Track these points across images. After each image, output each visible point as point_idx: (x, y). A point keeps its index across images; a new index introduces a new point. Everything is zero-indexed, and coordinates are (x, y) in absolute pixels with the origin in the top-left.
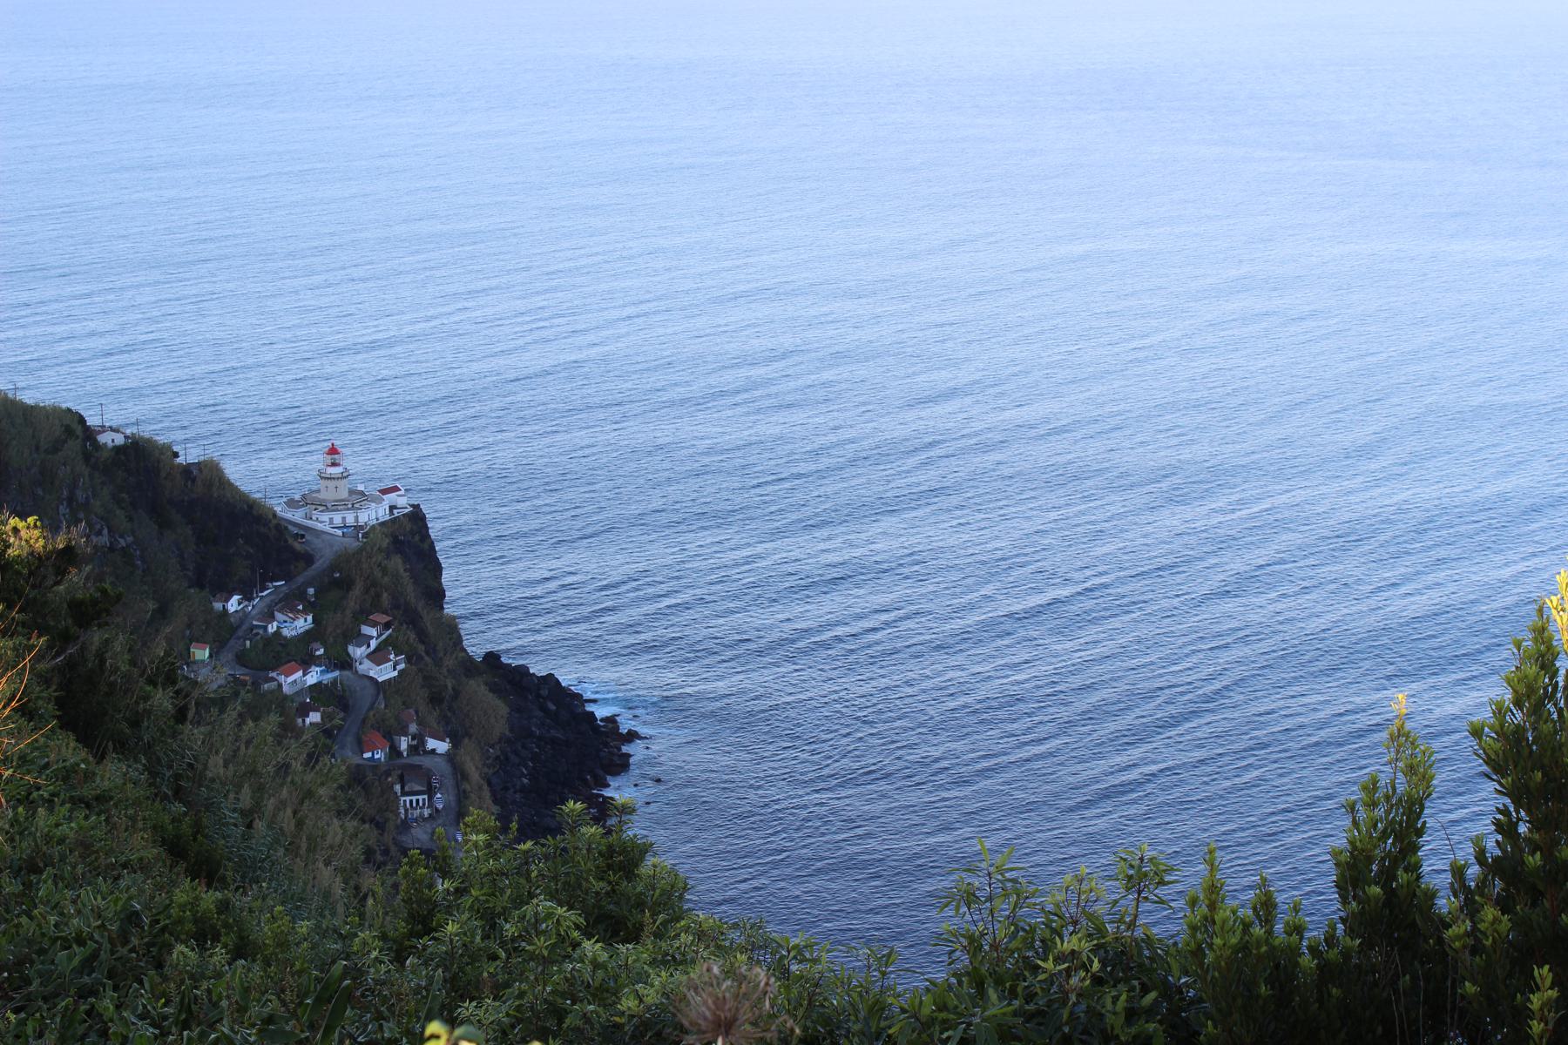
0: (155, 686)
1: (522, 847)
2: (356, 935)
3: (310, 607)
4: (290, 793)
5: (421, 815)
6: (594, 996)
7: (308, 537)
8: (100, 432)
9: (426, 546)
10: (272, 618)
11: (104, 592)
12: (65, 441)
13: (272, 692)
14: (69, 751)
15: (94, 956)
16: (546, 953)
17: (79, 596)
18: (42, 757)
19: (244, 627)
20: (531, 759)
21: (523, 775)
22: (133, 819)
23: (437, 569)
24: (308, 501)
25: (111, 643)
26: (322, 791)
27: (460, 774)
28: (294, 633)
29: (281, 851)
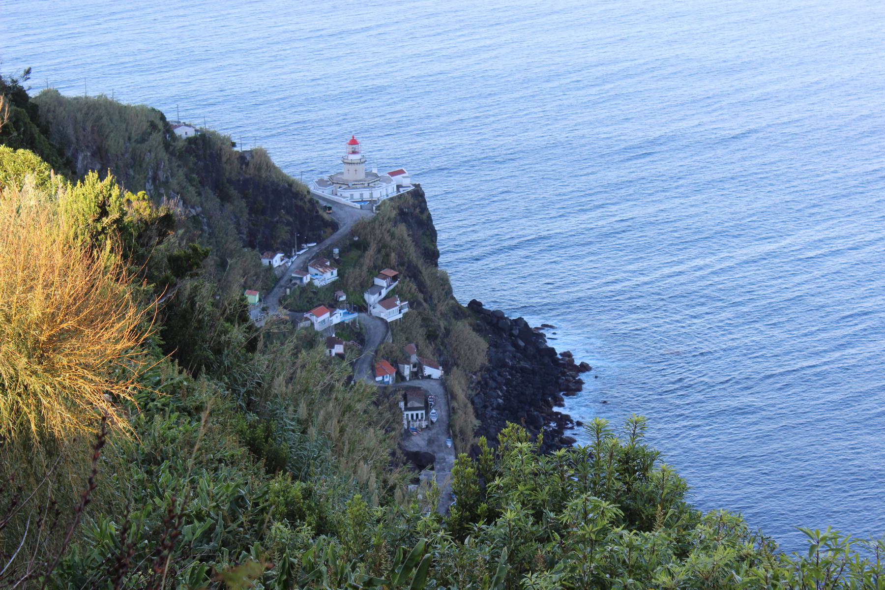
0: (232, 322)
1: (558, 453)
2: (418, 519)
3: (336, 263)
4: (334, 407)
5: (420, 427)
6: (630, 572)
7: (334, 209)
8: (176, 127)
9: (424, 217)
10: (306, 271)
11: (195, 250)
12: (151, 134)
13: (306, 329)
14: (171, 371)
15: (212, 529)
16: (593, 537)
17: (176, 252)
18: (155, 376)
19: (286, 278)
20: (505, 384)
21: (499, 396)
22: (224, 425)
23: (433, 234)
24: (333, 181)
25: (200, 288)
26: (358, 406)
27: (450, 395)
28: (323, 283)
29: (329, 452)
